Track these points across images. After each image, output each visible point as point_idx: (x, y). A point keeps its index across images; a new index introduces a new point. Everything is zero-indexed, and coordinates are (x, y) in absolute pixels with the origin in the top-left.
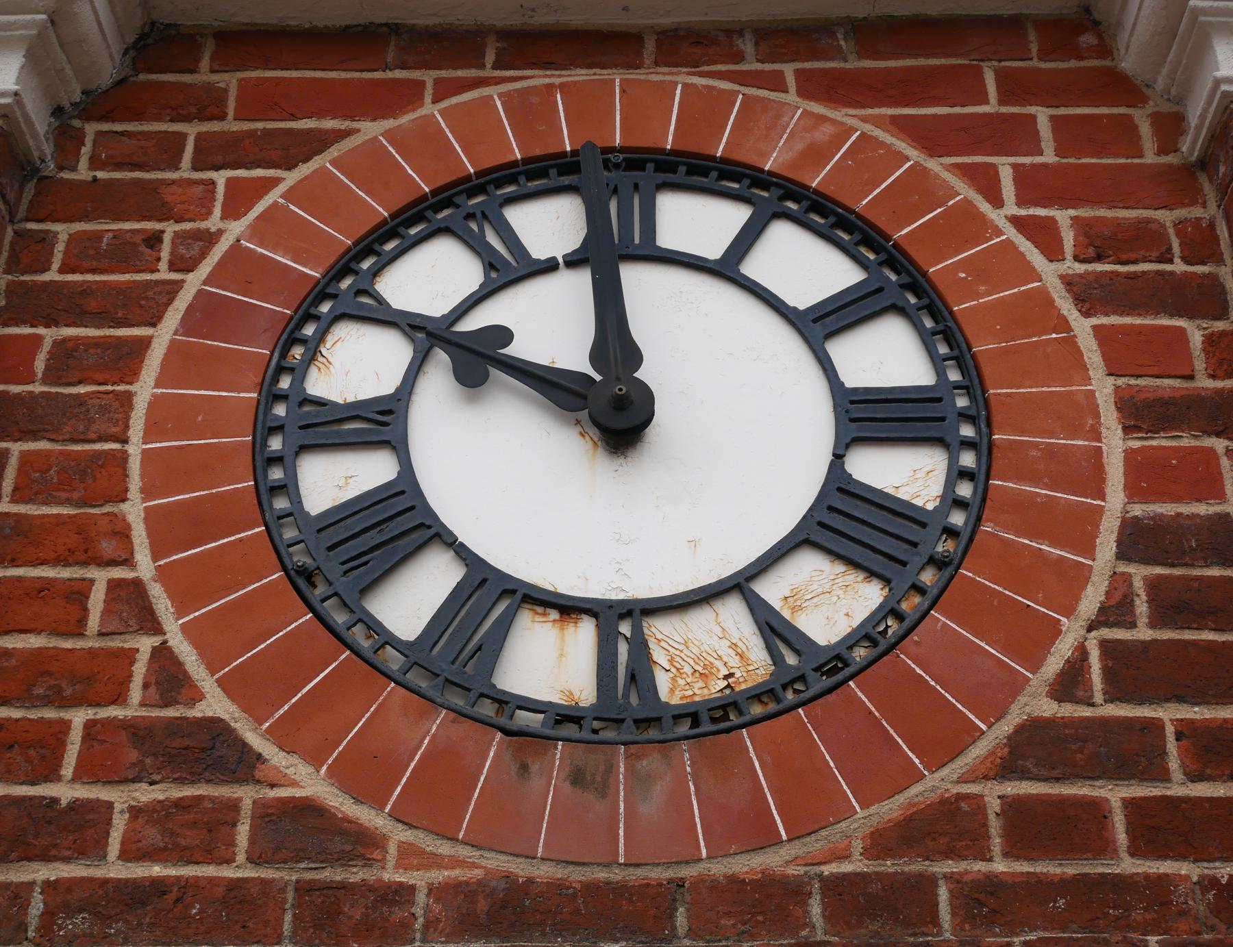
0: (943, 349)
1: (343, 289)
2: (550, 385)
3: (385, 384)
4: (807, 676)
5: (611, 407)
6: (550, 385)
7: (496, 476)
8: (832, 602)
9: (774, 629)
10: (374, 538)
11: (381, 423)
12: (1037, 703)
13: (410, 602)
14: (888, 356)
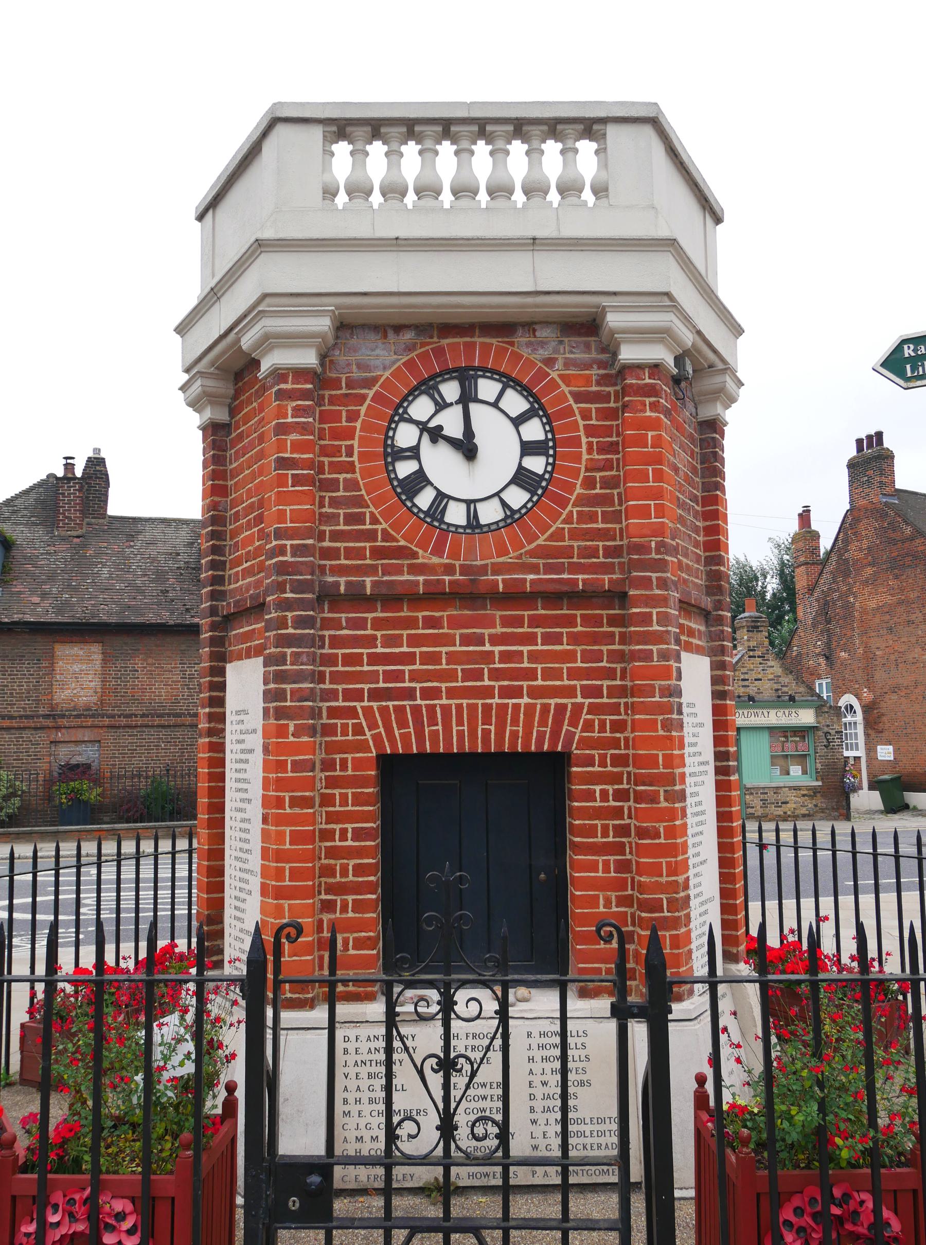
4: (511, 516)
5: (467, 448)
8: (517, 498)
9: (504, 504)
11: (414, 453)
12: (579, 490)
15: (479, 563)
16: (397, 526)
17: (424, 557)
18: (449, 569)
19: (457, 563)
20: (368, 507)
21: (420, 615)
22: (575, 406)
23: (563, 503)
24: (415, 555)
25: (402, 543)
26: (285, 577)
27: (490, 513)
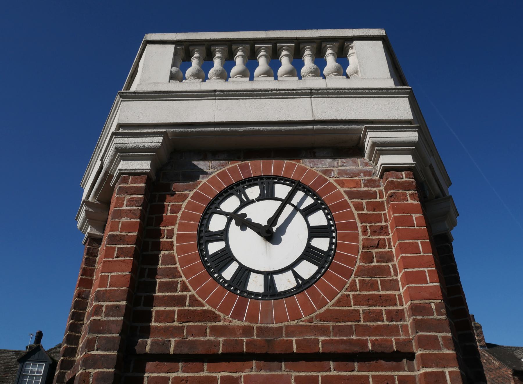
0: (329, 217)
1: (212, 207)
2: (257, 228)
3: (222, 227)
4: (303, 285)
5: (270, 234)
6: (257, 228)
7: (247, 248)
8: (307, 269)
9: (297, 276)
10: (222, 258)
11: (223, 235)
13: (256, 284)
14: (319, 219)
15: (275, 325)
16: (203, 293)
17: (227, 320)
18: (247, 331)
19: (255, 326)
20: (181, 277)
21: (219, 375)
22: (349, 201)
23: (347, 274)
24: (216, 318)
25: (207, 307)
26: (95, 335)
27: (284, 283)
